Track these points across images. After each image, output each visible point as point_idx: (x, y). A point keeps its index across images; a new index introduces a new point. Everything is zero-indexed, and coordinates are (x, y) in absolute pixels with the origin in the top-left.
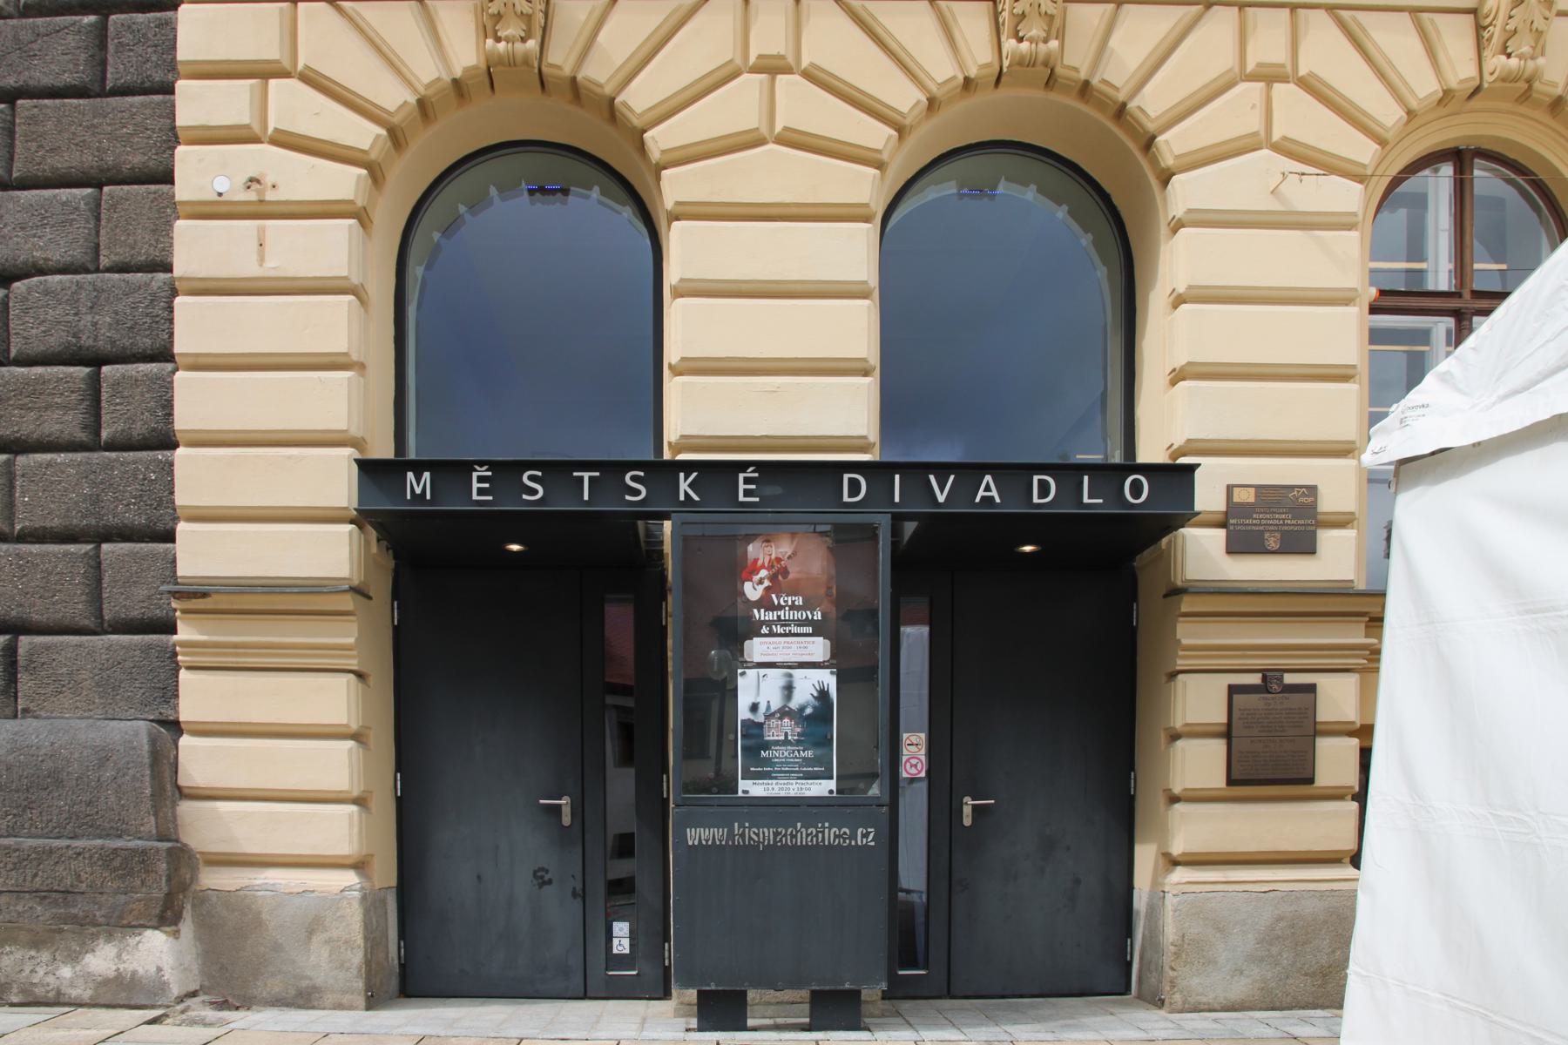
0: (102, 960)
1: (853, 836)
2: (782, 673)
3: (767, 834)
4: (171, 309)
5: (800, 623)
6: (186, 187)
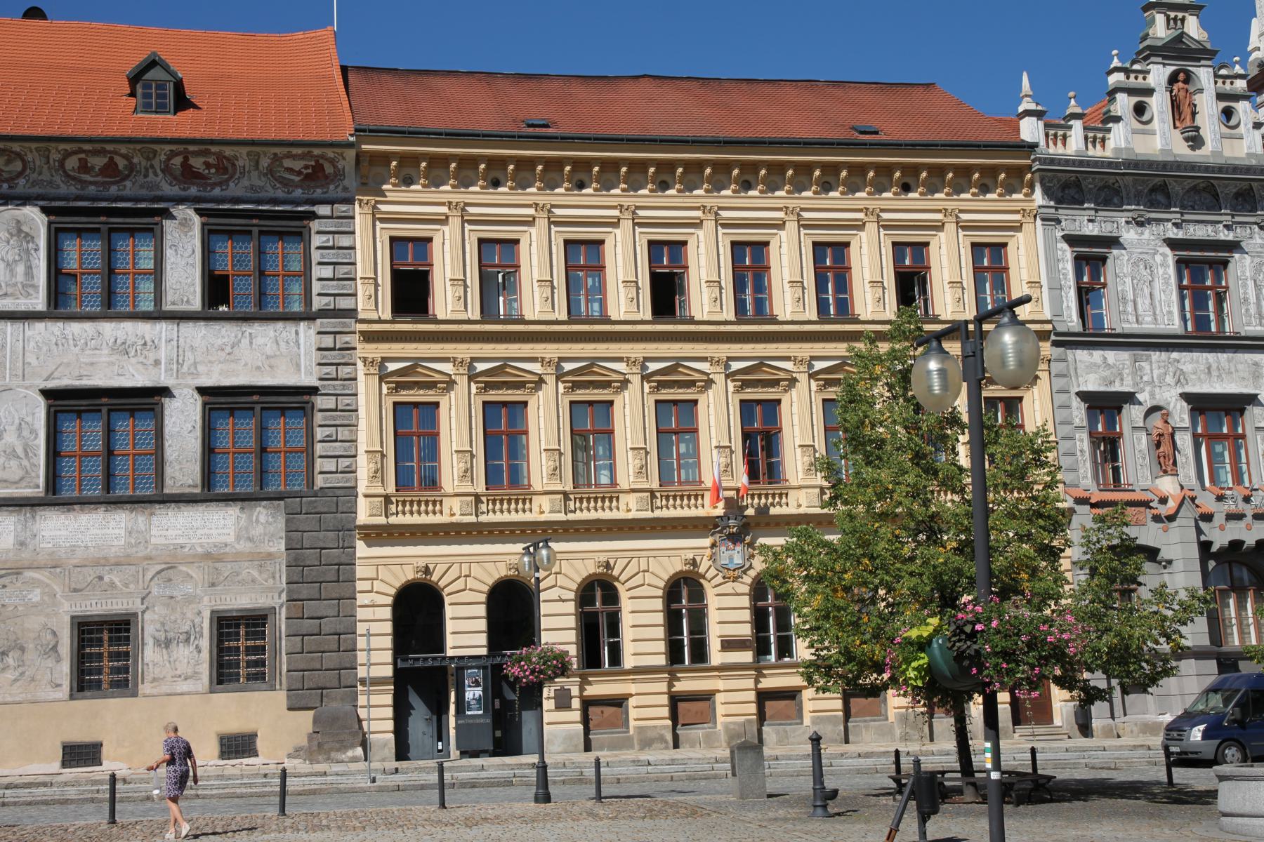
0: (350, 753)
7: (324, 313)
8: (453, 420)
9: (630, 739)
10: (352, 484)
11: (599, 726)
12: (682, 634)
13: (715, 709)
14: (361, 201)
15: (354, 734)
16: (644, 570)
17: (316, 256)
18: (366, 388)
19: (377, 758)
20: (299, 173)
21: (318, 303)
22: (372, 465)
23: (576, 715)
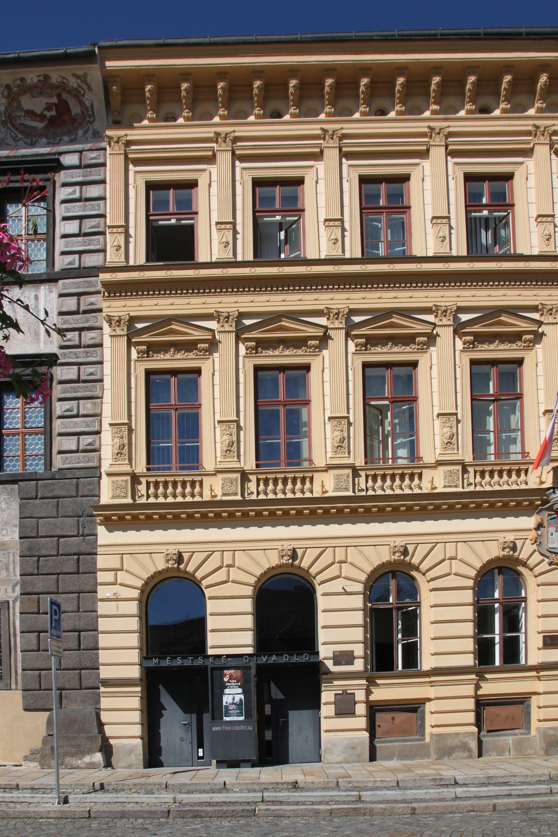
0: (87, 759)
1: (248, 728)
2: (232, 695)
3: (229, 728)
4: (98, 621)
5: (236, 686)
6: (100, 595)
7: (68, 273)
8: (217, 388)
9: (426, 747)
10: (94, 464)
11: (388, 733)
12: (493, 632)
13: (529, 714)
14: (110, 138)
15: (92, 739)
16: (450, 556)
17: (60, 211)
18: (112, 348)
19: (123, 764)
20: (42, 117)
21: (61, 262)
22: (116, 440)
23: (362, 722)
